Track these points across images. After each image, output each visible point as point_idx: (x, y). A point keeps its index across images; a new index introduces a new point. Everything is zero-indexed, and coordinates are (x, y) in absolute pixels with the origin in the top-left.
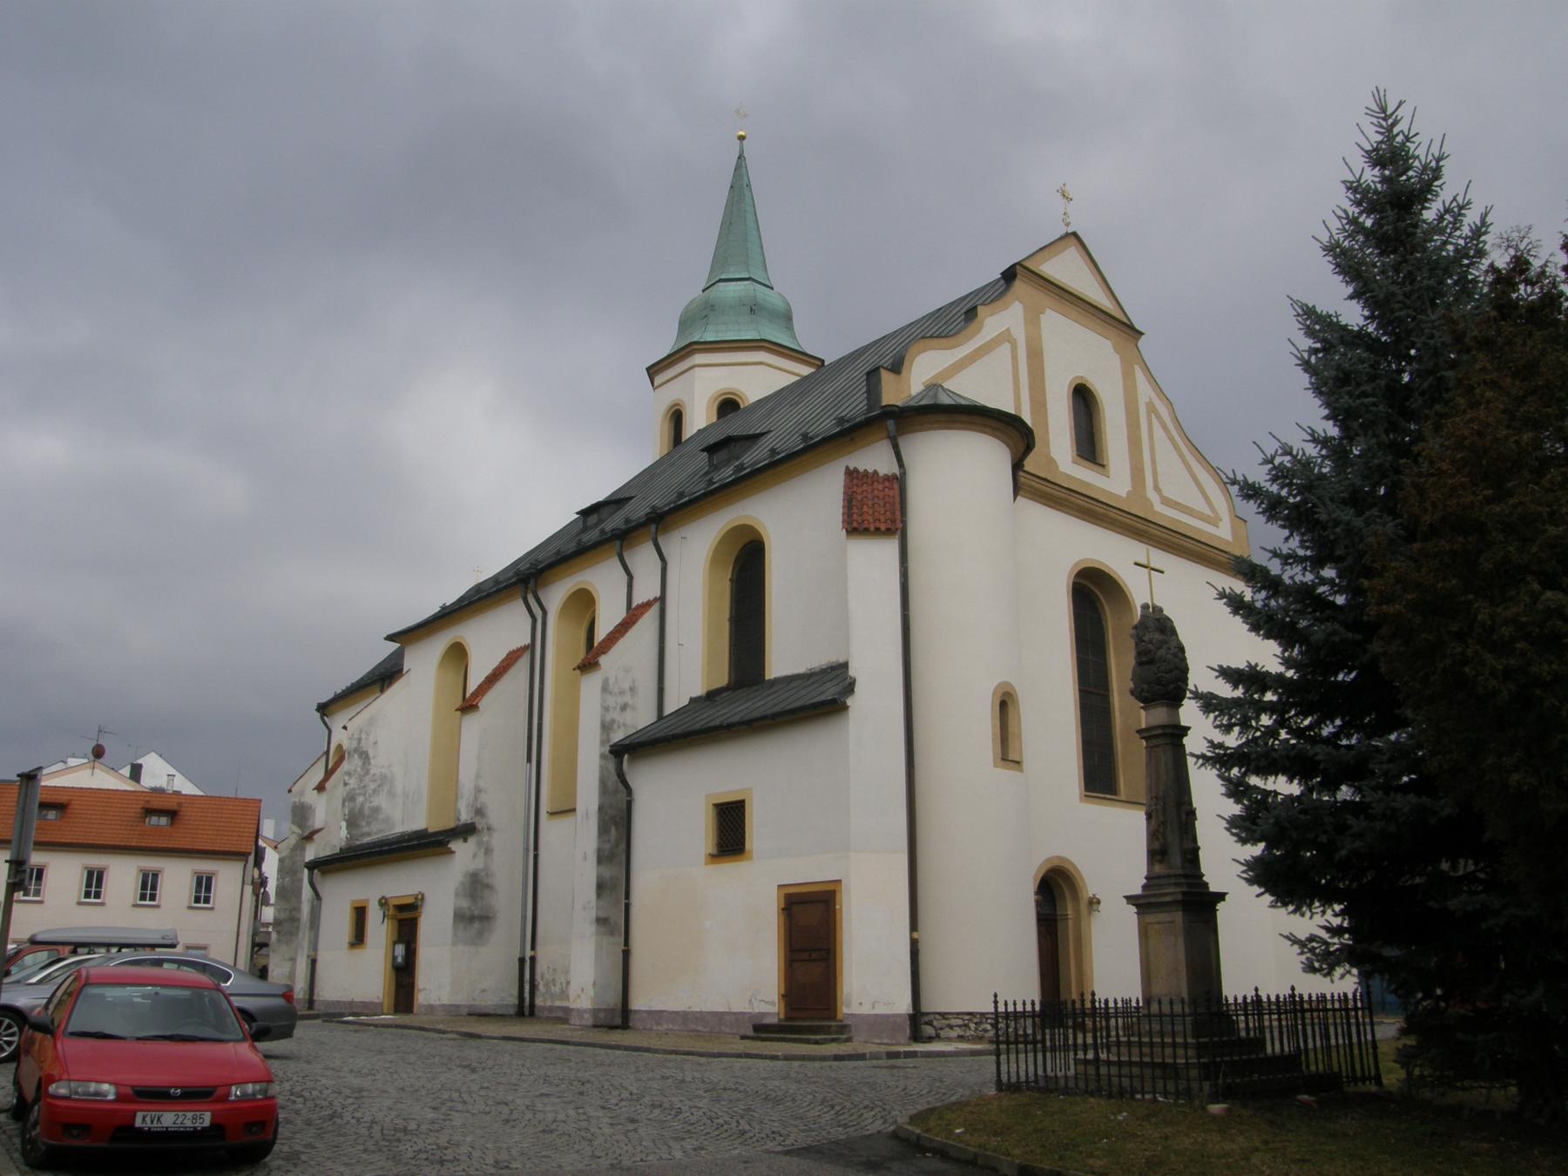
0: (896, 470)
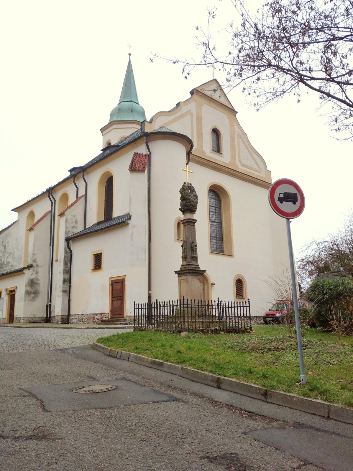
0: (148, 153)
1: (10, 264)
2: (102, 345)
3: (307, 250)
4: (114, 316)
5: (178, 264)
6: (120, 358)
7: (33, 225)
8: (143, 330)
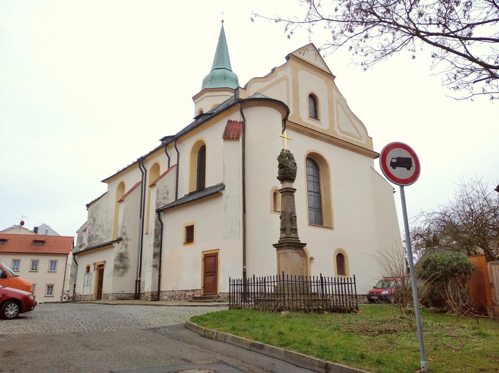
0: (242, 120)
1: (99, 238)
2: (196, 325)
3: (416, 222)
4: (206, 293)
5: (276, 236)
6: (216, 339)
7: (123, 197)
8: (239, 308)
